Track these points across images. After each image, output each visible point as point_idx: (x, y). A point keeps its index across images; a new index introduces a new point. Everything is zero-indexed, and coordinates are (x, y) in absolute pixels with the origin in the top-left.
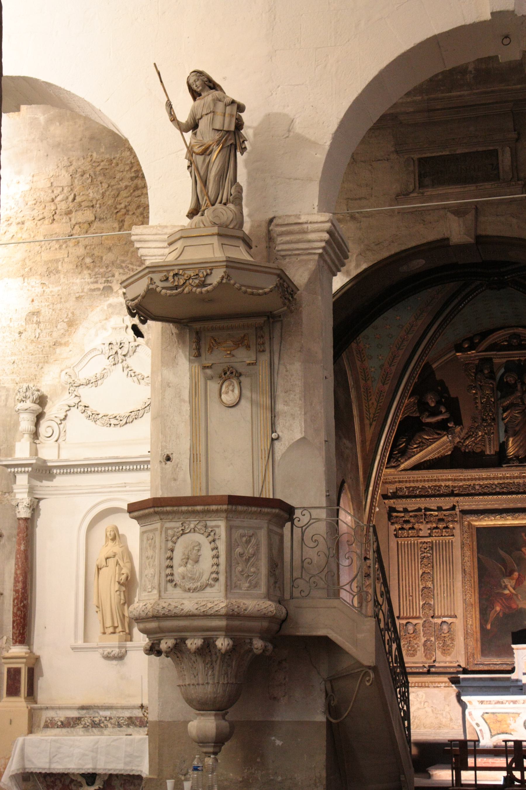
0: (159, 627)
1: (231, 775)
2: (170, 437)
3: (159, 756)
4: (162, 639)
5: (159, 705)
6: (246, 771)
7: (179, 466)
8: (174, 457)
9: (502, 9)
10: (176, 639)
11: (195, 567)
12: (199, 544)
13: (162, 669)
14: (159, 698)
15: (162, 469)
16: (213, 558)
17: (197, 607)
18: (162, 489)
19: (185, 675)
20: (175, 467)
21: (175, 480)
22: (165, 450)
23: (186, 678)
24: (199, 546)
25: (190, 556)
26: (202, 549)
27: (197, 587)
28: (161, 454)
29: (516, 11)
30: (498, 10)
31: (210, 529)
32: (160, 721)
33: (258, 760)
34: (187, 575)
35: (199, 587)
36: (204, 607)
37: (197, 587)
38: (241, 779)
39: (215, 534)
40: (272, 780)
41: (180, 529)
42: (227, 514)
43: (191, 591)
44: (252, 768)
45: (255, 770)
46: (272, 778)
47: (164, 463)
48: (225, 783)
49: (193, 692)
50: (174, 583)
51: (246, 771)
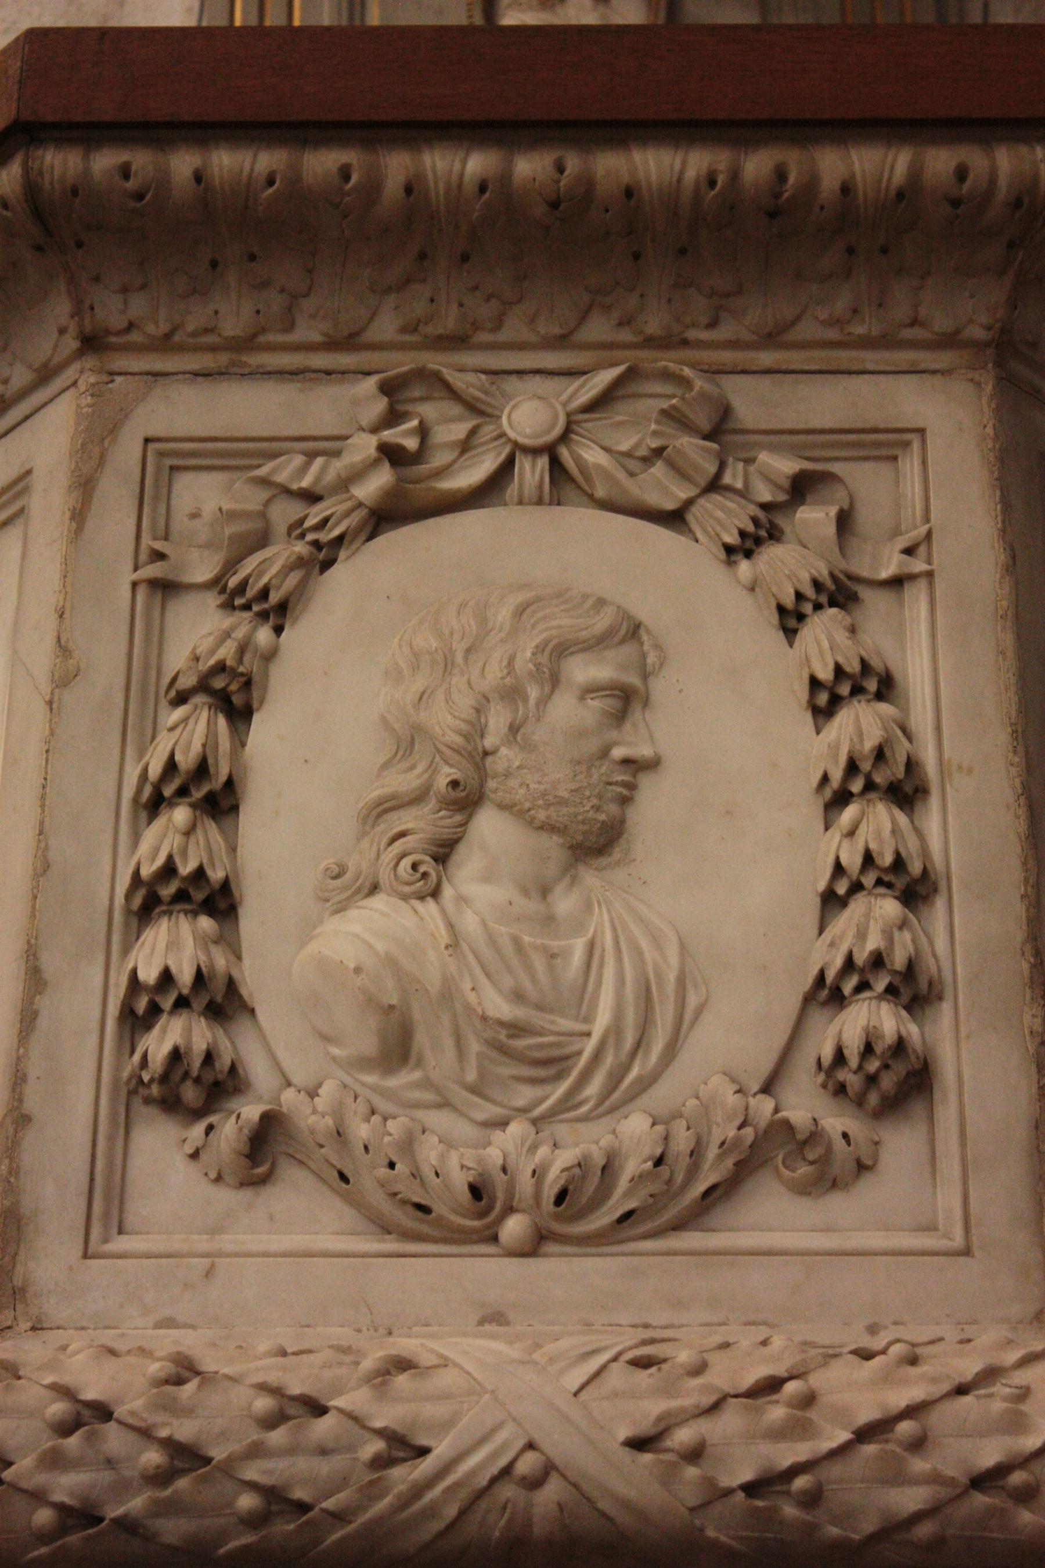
9: (332, 569)
11: (565, 903)
12: (634, 631)
16: (841, 799)
17: (653, 1408)
24: (628, 650)
25: (507, 757)
26: (658, 687)
27: (609, 1169)
29: (502, 1133)
30: (254, 555)
31: (786, 466)
34: (448, 993)
35: (632, 1166)
36: (776, 1412)
37: (609, 1169)
39: (844, 521)
41: (365, 446)
42: (1013, 304)
43: (514, 1227)
50: (251, 1112)
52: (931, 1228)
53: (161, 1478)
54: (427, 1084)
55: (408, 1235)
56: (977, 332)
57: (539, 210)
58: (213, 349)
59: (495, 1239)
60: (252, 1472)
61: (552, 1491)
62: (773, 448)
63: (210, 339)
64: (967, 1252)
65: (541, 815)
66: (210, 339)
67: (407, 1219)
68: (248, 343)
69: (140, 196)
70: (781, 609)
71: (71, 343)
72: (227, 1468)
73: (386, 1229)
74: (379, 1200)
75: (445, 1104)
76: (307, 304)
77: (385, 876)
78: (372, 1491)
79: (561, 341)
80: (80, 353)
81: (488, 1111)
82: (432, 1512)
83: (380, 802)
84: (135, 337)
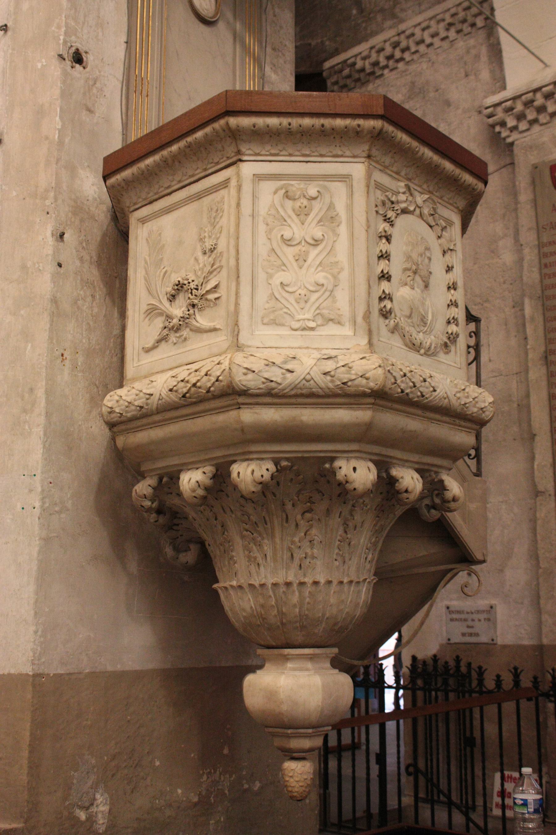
0: (369, 426)
1: (179, 791)
2: (85, 16)
3: (30, 768)
4: (235, 461)
5: (36, 632)
6: (205, 777)
7: (98, 85)
8: (89, 59)
10: (276, 462)
13: (47, 541)
14: (36, 613)
15: (65, 74)
18: (61, 118)
19: (313, 557)
20: (91, 83)
21: (90, 111)
22: (73, 38)
23: (318, 563)
28: (65, 42)
32: (36, 676)
33: (226, 751)
38: (196, 799)
40: (246, 791)
44: (215, 772)
45: (220, 774)
46: (246, 786)
47: (68, 63)
48: (168, 812)
49: (332, 601)
51: (205, 777)
52: (455, 363)
53: (411, 388)
54: (412, 322)
55: (410, 348)
56: (460, 208)
57: (433, 166)
58: (382, 166)
59: (419, 352)
60: (421, 389)
61: (447, 400)
62: (443, 220)
63: (383, 164)
64: (460, 368)
65: (424, 279)
66: (383, 164)
67: (411, 345)
68: (386, 167)
69: (393, 137)
70: (444, 251)
71: (365, 154)
72: (418, 388)
73: (406, 346)
74: (408, 340)
75: (414, 327)
76: (396, 164)
77: (408, 283)
78: (431, 395)
79: (420, 186)
80: (365, 157)
81: (418, 330)
82: (436, 400)
83: (405, 268)
84: (375, 159)
